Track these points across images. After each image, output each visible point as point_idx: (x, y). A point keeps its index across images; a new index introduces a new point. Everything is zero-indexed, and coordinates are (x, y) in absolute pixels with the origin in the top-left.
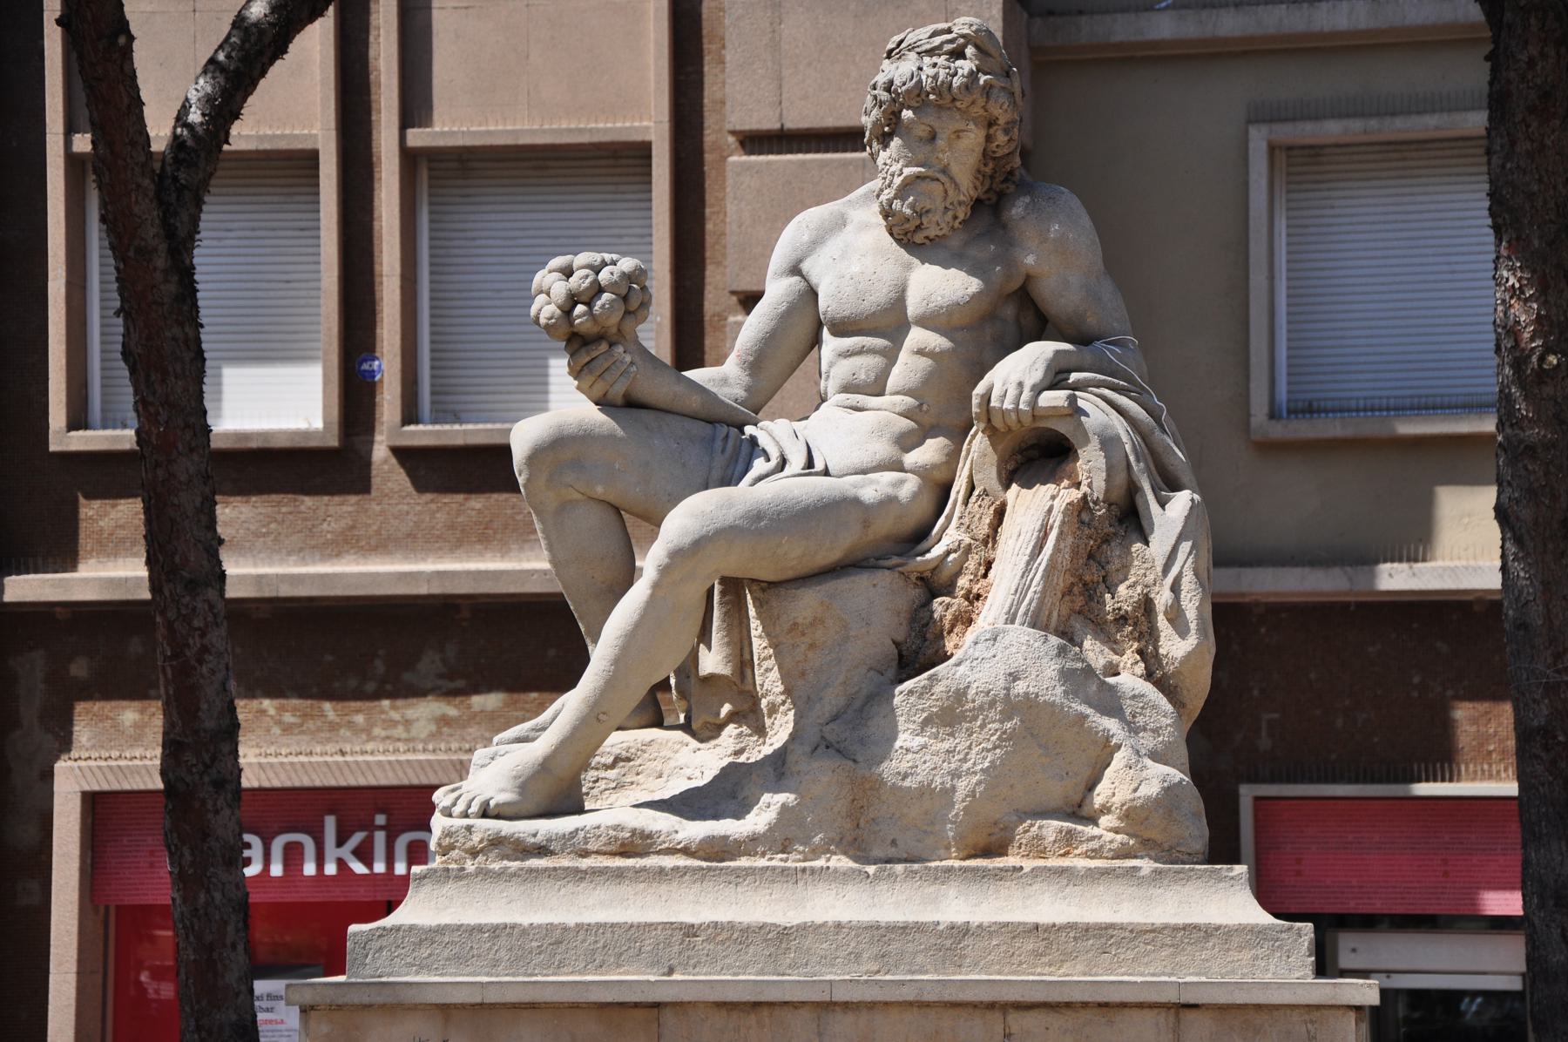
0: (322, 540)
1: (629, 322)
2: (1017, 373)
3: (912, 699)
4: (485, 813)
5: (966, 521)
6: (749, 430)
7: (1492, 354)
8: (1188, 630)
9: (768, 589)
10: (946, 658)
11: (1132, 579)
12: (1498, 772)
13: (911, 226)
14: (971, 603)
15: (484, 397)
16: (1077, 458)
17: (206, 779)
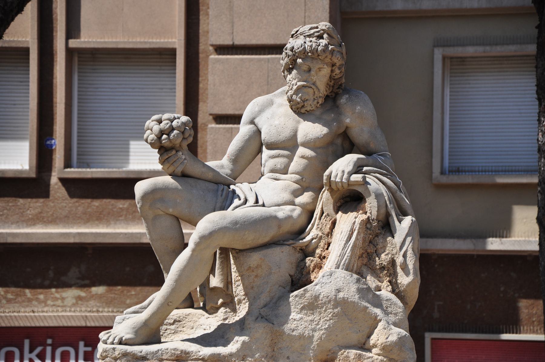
0: (27, 218)
2: (342, 167)
3: (297, 299)
4: (120, 343)
5: (320, 226)
6: (232, 187)
7: (536, 153)
8: (409, 273)
9: (239, 252)
11: (387, 252)
12: (537, 330)
13: (300, 106)
14: (321, 260)
15: (103, 157)
16: (365, 202)
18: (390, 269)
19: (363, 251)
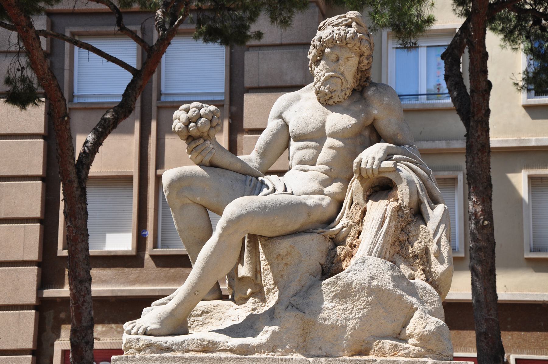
1: (212, 132)
2: (372, 155)
3: (329, 287)
4: (145, 334)
5: (350, 215)
8: (444, 261)
9: (268, 239)
10: (342, 270)
11: (420, 240)
14: (352, 249)
16: (397, 189)
17: (83, 341)
18: (423, 258)
19: (395, 239)
